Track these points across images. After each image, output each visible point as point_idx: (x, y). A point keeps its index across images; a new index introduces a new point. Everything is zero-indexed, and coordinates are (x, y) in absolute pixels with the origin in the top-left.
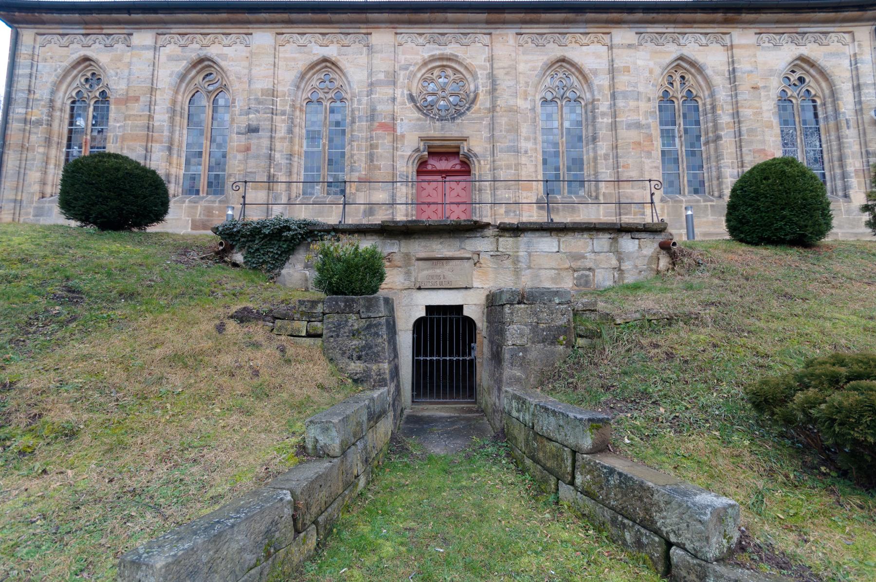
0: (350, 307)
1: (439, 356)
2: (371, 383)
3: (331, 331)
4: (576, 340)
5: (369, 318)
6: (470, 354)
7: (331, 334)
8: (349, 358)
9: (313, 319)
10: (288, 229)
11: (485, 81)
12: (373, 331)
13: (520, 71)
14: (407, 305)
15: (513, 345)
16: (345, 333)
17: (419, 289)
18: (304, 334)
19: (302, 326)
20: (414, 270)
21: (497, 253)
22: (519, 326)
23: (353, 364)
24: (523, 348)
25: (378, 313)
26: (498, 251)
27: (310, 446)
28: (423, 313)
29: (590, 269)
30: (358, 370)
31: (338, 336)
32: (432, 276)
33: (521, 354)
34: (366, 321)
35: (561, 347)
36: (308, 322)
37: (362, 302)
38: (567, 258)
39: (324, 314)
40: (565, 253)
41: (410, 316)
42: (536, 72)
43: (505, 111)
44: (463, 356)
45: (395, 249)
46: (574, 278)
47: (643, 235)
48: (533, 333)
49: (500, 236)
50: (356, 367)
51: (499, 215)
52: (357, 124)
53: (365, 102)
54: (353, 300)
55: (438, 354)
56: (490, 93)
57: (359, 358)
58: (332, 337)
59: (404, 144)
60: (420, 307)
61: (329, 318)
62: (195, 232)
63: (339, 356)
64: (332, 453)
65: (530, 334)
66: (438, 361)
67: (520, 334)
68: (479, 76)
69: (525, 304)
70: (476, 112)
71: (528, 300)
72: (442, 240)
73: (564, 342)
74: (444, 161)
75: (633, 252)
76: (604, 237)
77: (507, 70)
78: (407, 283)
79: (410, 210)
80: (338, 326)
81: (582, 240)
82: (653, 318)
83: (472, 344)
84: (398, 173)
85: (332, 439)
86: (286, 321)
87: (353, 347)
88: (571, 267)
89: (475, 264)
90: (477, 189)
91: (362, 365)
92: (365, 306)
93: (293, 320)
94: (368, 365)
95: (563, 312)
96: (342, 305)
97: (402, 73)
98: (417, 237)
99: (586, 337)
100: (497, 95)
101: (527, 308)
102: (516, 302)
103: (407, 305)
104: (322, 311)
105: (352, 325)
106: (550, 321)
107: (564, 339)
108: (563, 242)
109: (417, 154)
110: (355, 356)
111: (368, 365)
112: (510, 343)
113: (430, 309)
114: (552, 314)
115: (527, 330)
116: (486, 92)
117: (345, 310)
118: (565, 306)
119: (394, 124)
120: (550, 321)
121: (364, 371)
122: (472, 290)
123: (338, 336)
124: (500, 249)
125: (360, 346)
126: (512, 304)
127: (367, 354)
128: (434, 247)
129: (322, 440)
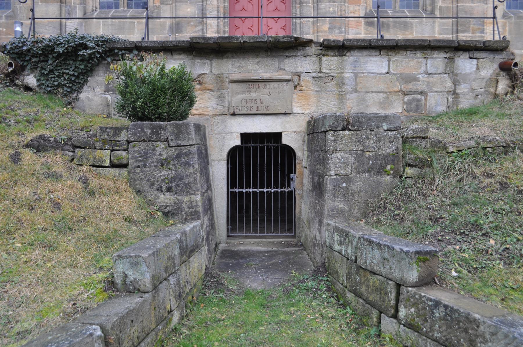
0: (158, 134)
3: (137, 161)
4: (404, 170)
5: (179, 146)
6: (289, 186)
7: (138, 164)
8: (158, 190)
9: (117, 148)
12: (183, 160)
15: (336, 175)
16: (153, 162)
17: (234, 114)
18: (107, 164)
22: (343, 154)
23: (162, 196)
24: (346, 178)
25: (188, 141)
27: (119, 281)
28: (237, 142)
29: (422, 93)
31: (145, 166)
34: (175, 150)
37: (170, 129)
38: (397, 80)
39: (129, 142)
40: (395, 74)
41: (224, 145)
44: (246, 188)
45: (206, 70)
46: (404, 103)
47: (483, 54)
48: (358, 162)
49: (324, 55)
51: (322, 32)
54: (160, 127)
57: (169, 190)
58: (138, 167)
60: (235, 135)
61: (134, 146)
63: (147, 188)
64: (142, 288)
65: (354, 163)
66: (255, 193)
67: (344, 163)
69: (350, 130)
72: (258, 60)
73: (392, 172)
75: (470, 74)
76: (440, 56)
78: (220, 108)
80: (145, 156)
81: (415, 60)
82: (488, 145)
83: (292, 175)
86: (87, 150)
87: (162, 178)
88: (401, 90)
89: (295, 87)
91: (172, 197)
92: (173, 132)
93: (95, 148)
94: (179, 198)
95: (392, 139)
96: (149, 132)
99: (415, 166)
101: (352, 135)
102: (339, 129)
104: (126, 139)
105: (160, 155)
106: (376, 149)
107: (391, 169)
108: (394, 61)
111: (179, 198)
112: (333, 173)
113: (245, 137)
115: (351, 159)
117: (151, 137)
118: (394, 133)
120: (376, 149)
121: (175, 203)
122: (291, 116)
123: (145, 166)
124: (324, 70)
127: (177, 185)
128: (250, 67)
129: (132, 275)
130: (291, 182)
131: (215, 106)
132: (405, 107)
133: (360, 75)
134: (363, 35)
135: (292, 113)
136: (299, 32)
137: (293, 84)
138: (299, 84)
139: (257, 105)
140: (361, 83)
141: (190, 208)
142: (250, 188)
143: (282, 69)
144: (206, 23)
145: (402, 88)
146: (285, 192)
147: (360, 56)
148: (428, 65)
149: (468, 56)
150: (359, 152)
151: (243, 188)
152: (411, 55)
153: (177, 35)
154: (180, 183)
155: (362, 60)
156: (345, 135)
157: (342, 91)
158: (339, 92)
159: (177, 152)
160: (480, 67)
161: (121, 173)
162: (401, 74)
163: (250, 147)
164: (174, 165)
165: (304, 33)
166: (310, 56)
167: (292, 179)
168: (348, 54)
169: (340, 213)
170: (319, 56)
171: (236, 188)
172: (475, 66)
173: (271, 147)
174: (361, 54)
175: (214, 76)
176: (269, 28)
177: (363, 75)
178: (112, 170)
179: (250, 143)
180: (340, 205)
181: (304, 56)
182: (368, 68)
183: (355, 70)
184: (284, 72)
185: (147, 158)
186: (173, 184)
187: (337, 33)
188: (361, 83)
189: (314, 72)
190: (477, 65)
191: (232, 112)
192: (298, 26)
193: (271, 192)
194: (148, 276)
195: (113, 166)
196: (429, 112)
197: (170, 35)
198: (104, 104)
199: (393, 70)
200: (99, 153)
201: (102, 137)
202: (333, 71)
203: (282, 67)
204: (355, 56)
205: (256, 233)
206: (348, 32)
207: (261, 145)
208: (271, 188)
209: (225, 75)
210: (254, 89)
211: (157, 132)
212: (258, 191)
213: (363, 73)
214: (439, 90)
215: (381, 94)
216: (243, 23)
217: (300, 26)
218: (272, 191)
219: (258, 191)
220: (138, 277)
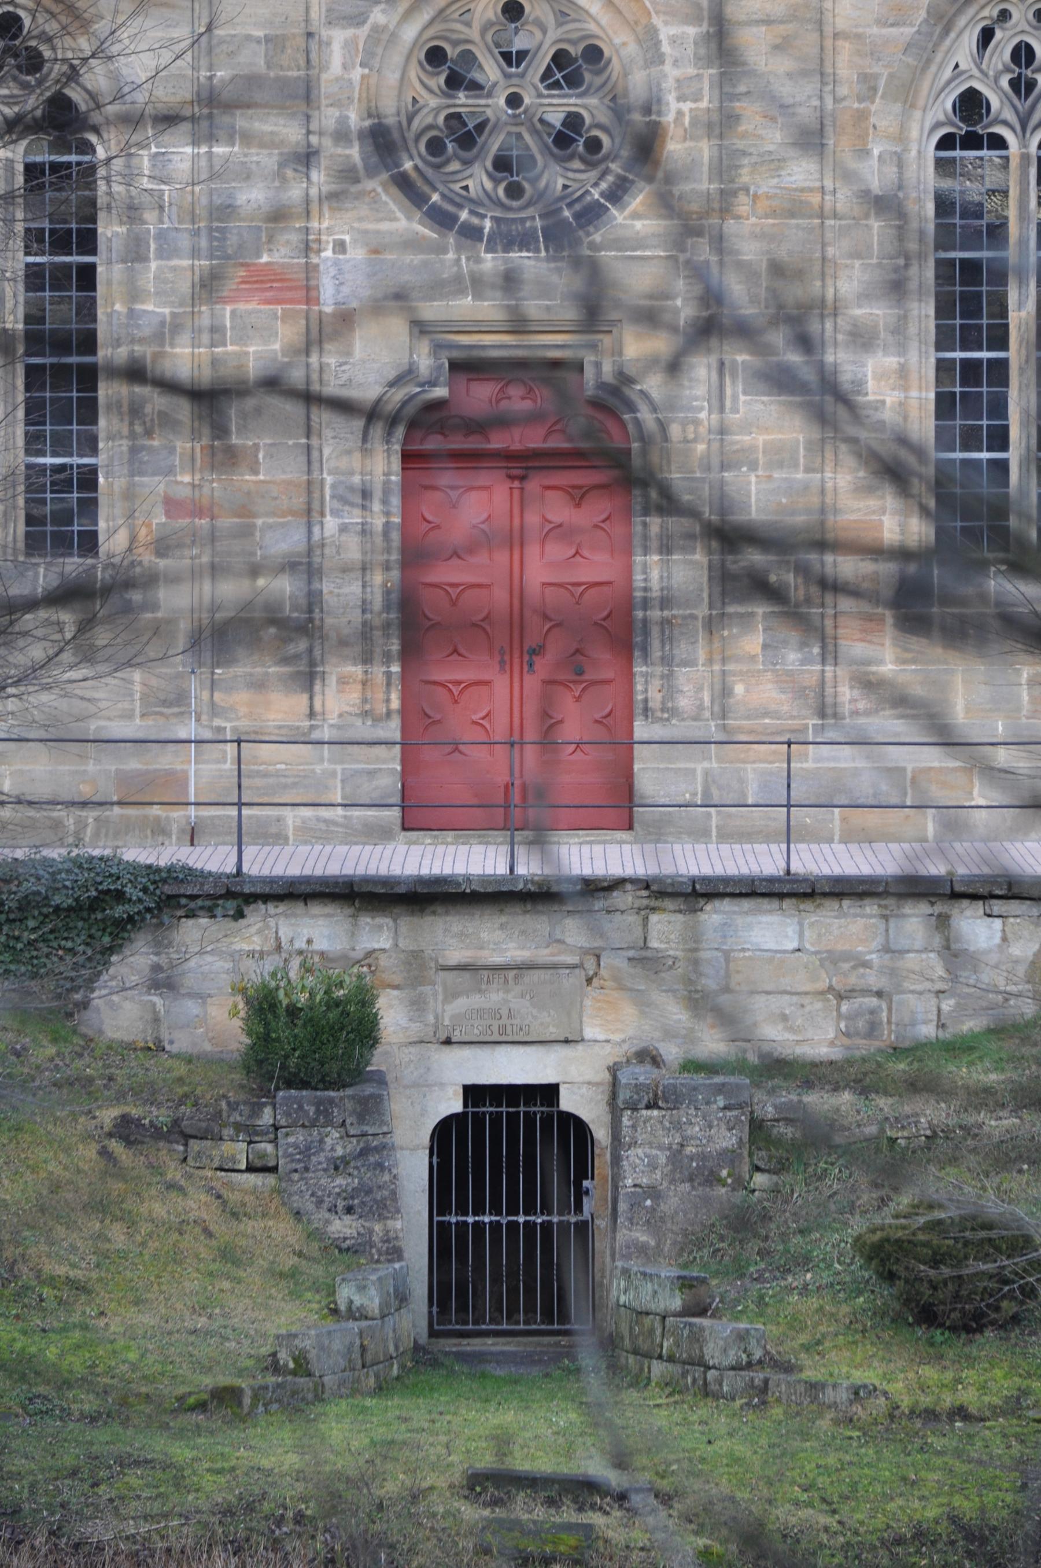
0: (327, 1114)
1: (499, 1213)
2: (372, 1255)
3: (293, 1161)
4: (751, 1178)
5: (364, 1135)
6: (579, 1208)
7: (294, 1166)
8: (330, 1210)
9: (257, 1139)
10: (119, 896)
11: (691, 71)
12: (372, 1159)
13: (841, 24)
14: (415, 1085)
15: (635, 1186)
16: (320, 1163)
17: (448, 1042)
18: (243, 1167)
19: (238, 1151)
20: (435, 994)
21: (644, 953)
22: (648, 1151)
23: (338, 1222)
24: (653, 1192)
25: (380, 1126)
26: (645, 947)
27: (343, 1308)
28: (456, 1106)
29: (879, 994)
30: (348, 1232)
31: (307, 1169)
32: (480, 1012)
33: (648, 1202)
34: (358, 1142)
35: (723, 1190)
36: (250, 1143)
37: (349, 1105)
38: (822, 966)
39: (276, 1128)
40: (816, 953)
41: (424, 1112)
42: (908, 31)
43: (773, 213)
44: (475, 1214)
45: (383, 941)
46: (840, 1016)
47: (1014, 907)
48: (673, 1164)
49: (653, 909)
50: (342, 1227)
51: (738, 659)
52: (153, 265)
53: (186, 166)
54: (331, 1101)
55: (496, 1210)
56: (710, 126)
57: (349, 1210)
58: (296, 1171)
60: (450, 1091)
61: (287, 1135)
62: (692, 765)
63: (310, 1207)
64: (370, 1314)
65: (667, 1165)
66: (496, 1226)
67: (648, 1165)
68: (666, 48)
69: (659, 1108)
71: (667, 1102)
72: (503, 919)
73: (729, 1181)
75: (989, 951)
76: (917, 911)
77: (782, 29)
78: (415, 1027)
80: (306, 1152)
81: (861, 921)
82: (900, 1134)
83: (586, 1183)
84: (329, 480)
85: (371, 1299)
86: (209, 1143)
87: (337, 1190)
88: (831, 989)
89: (589, 981)
91: (354, 1224)
92: (354, 1111)
93: (221, 1139)
94: (367, 1224)
95: (731, 1124)
96: (311, 1110)
97: (338, 37)
98: (440, 909)
99: (768, 1171)
100: (740, 144)
101: (664, 1116)
102: (643, 1105)
103: (415, 1085)
104: (271, 1122)
105: (333, 1149)
106: (704, 1141)
107: (729, 1175)
108: (812, 924)
110: (340, 1208)
111: (367, 1224)
112: (629, 1182)
113: (473, 1093)
114: (710, 1127)
115: (662, 1159)
116: (694, 122)
117: (316, 1120)
118: (735, 1113)
119: (311, 270)
120: (704, 1141)
121: (359, 1234)
122: (580, 1047)
123: (307, 1169)
124: (654, 944)
125: (350, 1189)
126: (635, 1109)
127: (363, 1203)
128: (484, 935)
129: (358, 1300)
130: (585, 1200)
131: (404, 1022)
132: (842, 1025)
133: (736, 954)
134: (890, 667)
135: (583, 1040)
136: (659, 654)
137: (583, 973)
138: (596, 974)
139: (501, 1022)
140: (738, 972)
141: (384, 1242)
142: (484, 1214)
143: (559, 941)
144: (321, 628)
145: (834, 982)
146: (569, 1223)
147: (735, 913)
148: (891, 931)
149: (981, 912)
150: (675, 1147)
151: (467, 1215)
152: (852, 911)
153: (218, 671)
154: (367, 1199)
155: (740, 920)
156: (651, 1118)
157: (697, 991)
158: (690, 992)
159: (362, 1145)
160: (1009, 935)
161: (267, 1181)
162: (828, 951)
163: (484, 1113)
164: (356, 1168)
165: (677, 660)
166: (622, 912)
167: (587, 1192)
168: (708, 907)
169: (642, 1250)
170: (643, 913)
171: (450, 1214)
172: (999, 935)
173: (535, 1113)
174: (736, 909)
175: (402, 956)
176: (549, 526)
177: (742, 955)
178: (253, 1179)
179: (484, 1105)
180: (643, 1237)
181: (609, 912)
182: (754, 940)
183: (725, 943)
184: (563, 947)
185: (309, 1156)
186: (356, 1201)
187: (793, 664)
188: (738, 972)
189: (632, 948)
190: (1004, 931)
191: (443, 1038)
192: (655, 632)
193: (535, 1224)
194: (377, 1301)
195: (251, 1169)
196: (897, 1038)
197: (193, 672)
198: (149, 1016)
199: (812, 945)
200: (227, 1147)
201: (232, 1119)
202: (673, 945)
203: (558, 937)
204: (725, 913)
205: (498, 1324)
206: (836, 658)
207: (511, 1110)
208: (535, 1214)
209: (428, 952)
210: (495, 986)
211: (326, 1110)
212: (504, 1221)
213: (743, 950)
214: (918, 987)
215: (787, 997)
216: (456, 702)
217: (663, 632)
218: (539, 1221)
219: (504, 1221)
220: (366, 1302)
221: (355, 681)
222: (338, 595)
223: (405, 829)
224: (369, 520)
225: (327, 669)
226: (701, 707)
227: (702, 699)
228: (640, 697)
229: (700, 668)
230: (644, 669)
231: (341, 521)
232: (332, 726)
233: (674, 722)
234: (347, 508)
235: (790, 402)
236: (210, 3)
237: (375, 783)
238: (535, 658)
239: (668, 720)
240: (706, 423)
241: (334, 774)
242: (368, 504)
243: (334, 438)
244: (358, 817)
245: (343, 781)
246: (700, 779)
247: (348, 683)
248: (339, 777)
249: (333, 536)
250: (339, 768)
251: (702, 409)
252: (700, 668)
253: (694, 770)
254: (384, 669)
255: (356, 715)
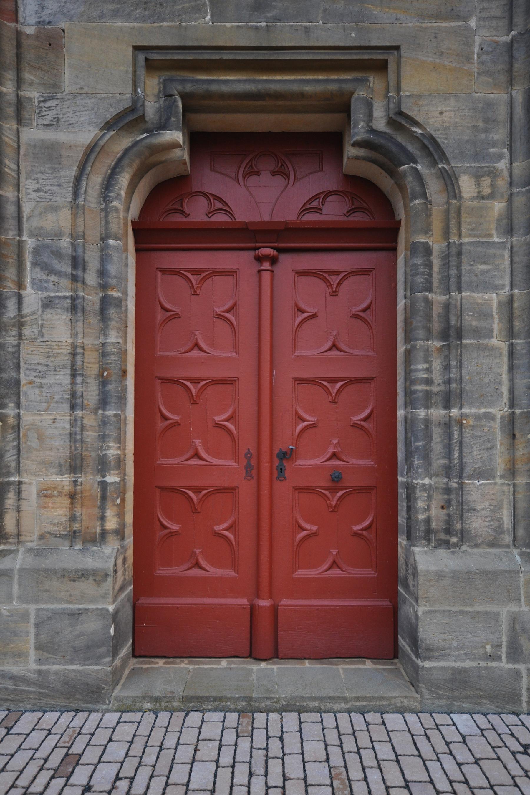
59: (56, 86)
62: (493, 608)
70: (372, 322)
74: (265, 177)
79: (91, 435)
84: (30, 243)
90: (436, 326)
109: (126, 142)
165: (468, 470)
216: (196, 511)
221: (60, 493)
222: (41, 386)
223: (134, 656)
224: (81, 293)
225: (25, 478)
226: (499, 530)
227: (500, 520)
228: (421, 517)
229: (498, 480)
230: (427, 481)
231: (45, 294)
232: (30, 550)
233: (464, 548)
234: (53, 278)
235: (123, 685)
236: (370, 792)
237: (79, 628)
238: (285, 463)
239: (456, 545)
240: (506, 174)
241: (25, 616)
242: (79, 273)
243: (37, 191)
244: (56, 673)
245: (37, 625)
246: (504, 626)
247: (51, 496)
248: (32, 620)
249: (34, 313)
250: (32, 608)
251: (501, 157)
252: (498, 480)
253: (497, 615)
254: (99, 478)
255: (62, 536)
